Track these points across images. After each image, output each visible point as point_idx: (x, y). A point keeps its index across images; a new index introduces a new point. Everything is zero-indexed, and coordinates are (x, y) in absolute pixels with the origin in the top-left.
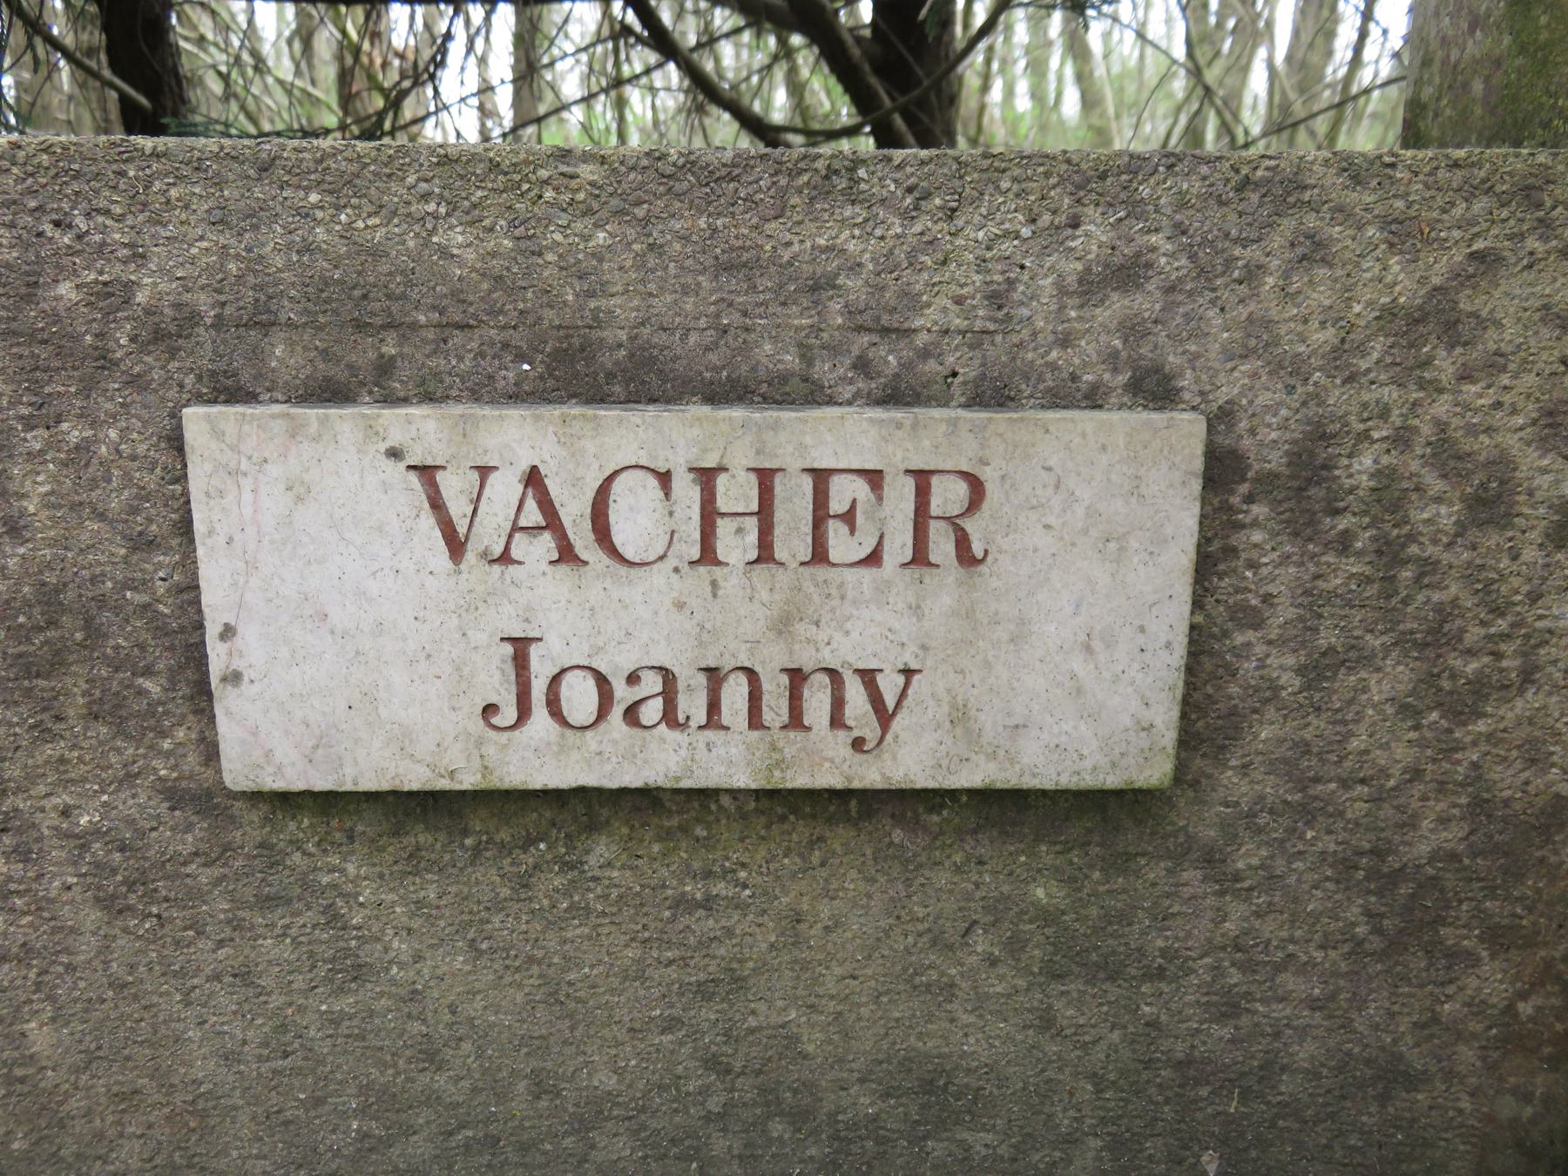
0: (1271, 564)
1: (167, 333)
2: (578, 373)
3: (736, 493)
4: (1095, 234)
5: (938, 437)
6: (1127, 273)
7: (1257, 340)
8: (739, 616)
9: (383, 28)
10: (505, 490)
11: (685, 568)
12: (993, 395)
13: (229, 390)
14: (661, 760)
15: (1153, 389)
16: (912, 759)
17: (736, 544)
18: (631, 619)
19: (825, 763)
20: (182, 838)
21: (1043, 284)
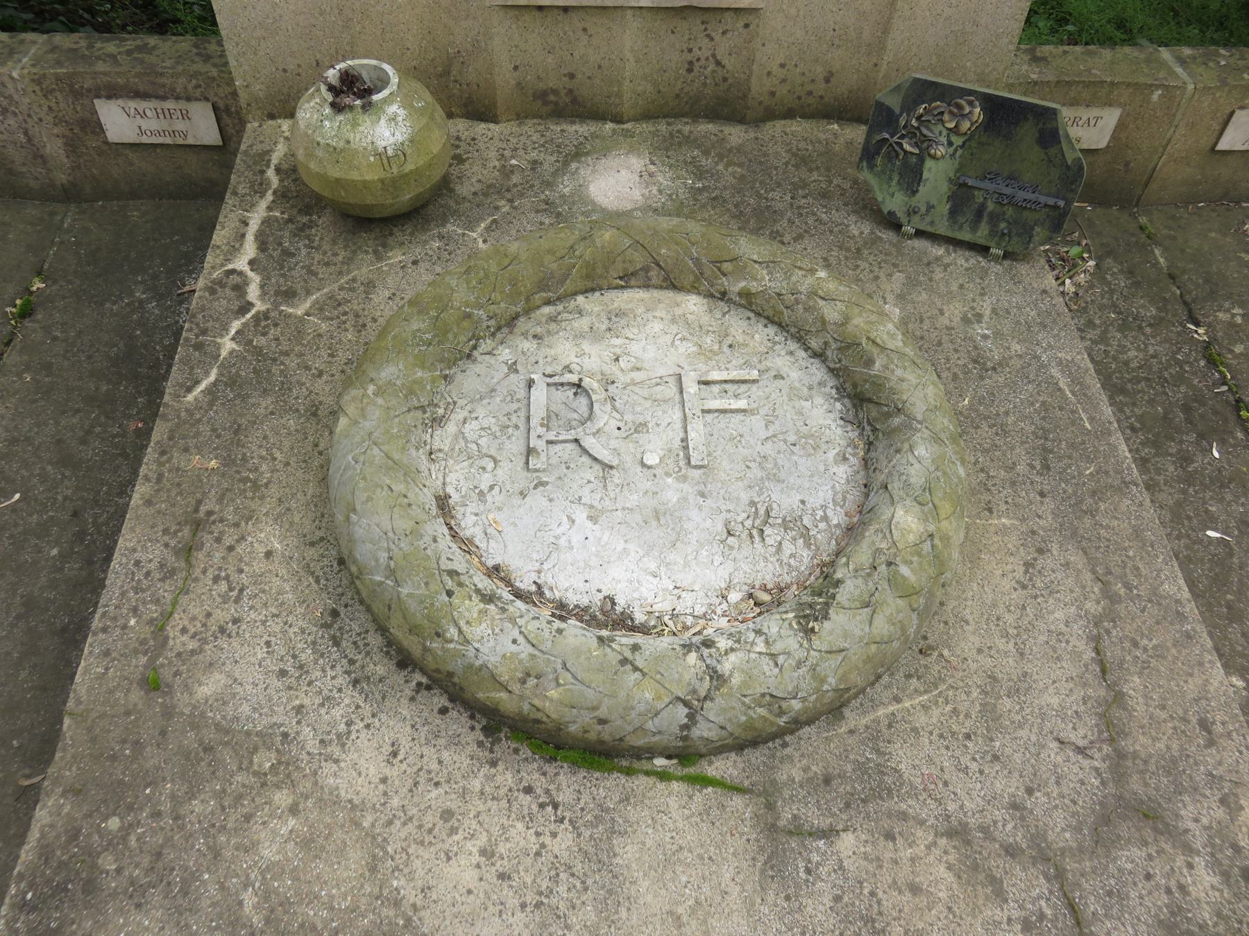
0: (226, 119)
1: (89, 90)
2: (144, 96)
3: (159, 111)
4: (194, 82)
5: (182, 105)
6: (200, 86)
7: (216, 94)
8: (162, 124)
9: (761, 240)
10: (132, 110)
11: (689, 57)
12: (188, 99)
13: (98, 97)
14: (160, 140)
15: (207, 99)
16: (190, 141)
17: (161, 116)
18: (151, 124)
19: (180, 141)
20: (105, 148)
21: (190, 87)
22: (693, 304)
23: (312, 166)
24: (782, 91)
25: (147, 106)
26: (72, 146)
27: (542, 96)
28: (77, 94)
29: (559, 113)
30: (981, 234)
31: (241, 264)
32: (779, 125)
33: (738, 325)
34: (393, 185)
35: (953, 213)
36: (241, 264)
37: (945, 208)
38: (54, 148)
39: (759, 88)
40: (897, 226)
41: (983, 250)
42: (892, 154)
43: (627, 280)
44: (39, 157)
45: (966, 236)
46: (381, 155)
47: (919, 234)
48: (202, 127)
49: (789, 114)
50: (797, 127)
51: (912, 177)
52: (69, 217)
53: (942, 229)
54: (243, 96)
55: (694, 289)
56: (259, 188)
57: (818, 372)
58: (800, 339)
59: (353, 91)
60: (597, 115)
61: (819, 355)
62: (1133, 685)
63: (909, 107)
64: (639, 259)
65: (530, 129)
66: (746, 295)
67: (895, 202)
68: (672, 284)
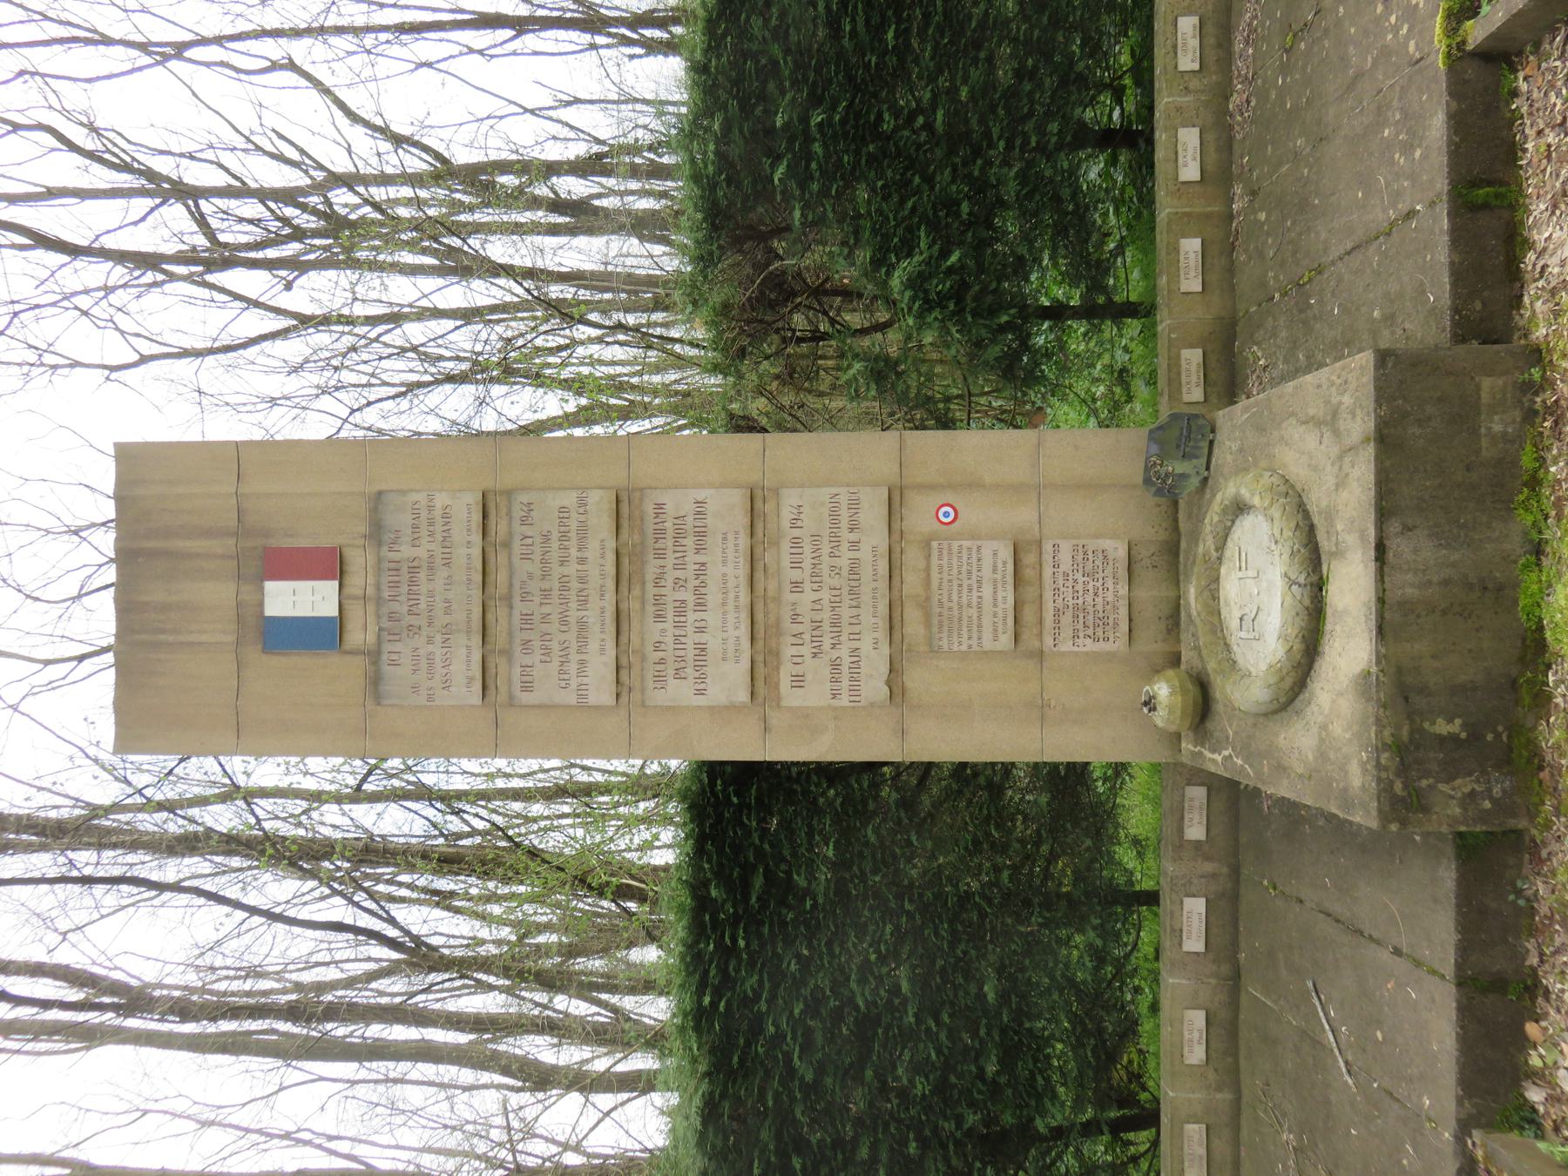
18: (1196, 818)
22: (1223, 571)
23: (432, 212)
24: (1164, 525)
25: (1187, 817)
26: (1208, 858)
27: (1169, 631)
28: (1181, 846)
29: (1177, 624)
30: (1205, 445)
31: (1219, 758)
32: (1181, 525)
33: (1231, 550)
34: (1184, 691)
35: (1196, 457)
36: (1219, 758)
37: (1195, 461)
38: (1209, 867)
39: (1163, 536)
40: (1206, 479)
41: (1211, 443)
42: (1171, 487)
43: (1215, 597)
44: (1214, 876)
45: (1206, 451)
46: (1171, 694)
47: (1208, 468)
48: (1197, 794)
49: (1176, 520)
50: (1181, 516)
51: (1183, 476)
52: (1245, 871)
53: (1204, 461)
54: (1170, 760)
55: (1218, 570)
56: (1200, 753)
57: (1238, 522)
58: (1230, 528)
59: (1150, 703)
60: (1178, 606)
61: (1233, 522)
62: (1311, 412)
63: (1153, 484)
64: (1207, 593)
65: (1183, 636)
66: (1217, 550)
67: (1194, 482)
68: (1217, 579)
